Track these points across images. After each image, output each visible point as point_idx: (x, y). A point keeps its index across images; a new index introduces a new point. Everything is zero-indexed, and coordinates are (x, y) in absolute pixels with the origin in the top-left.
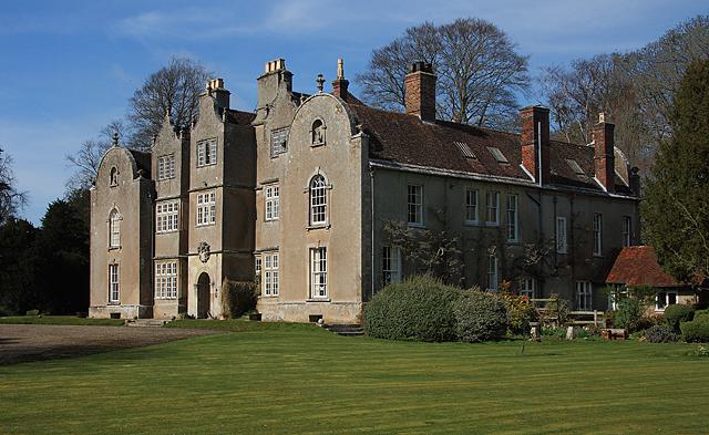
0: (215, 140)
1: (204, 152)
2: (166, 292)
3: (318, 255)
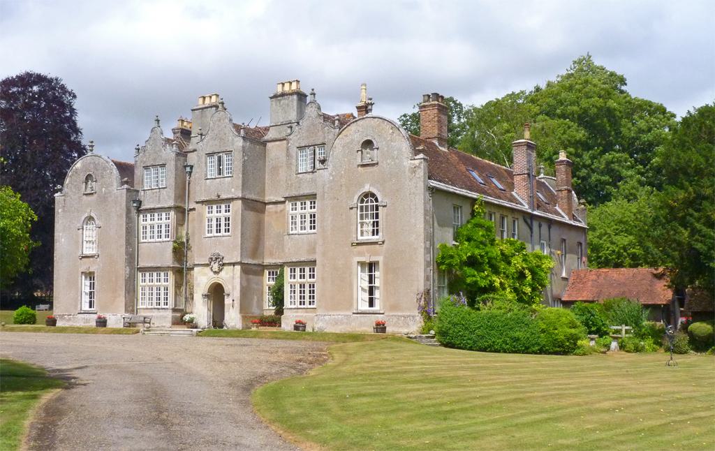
0: (229, 152)
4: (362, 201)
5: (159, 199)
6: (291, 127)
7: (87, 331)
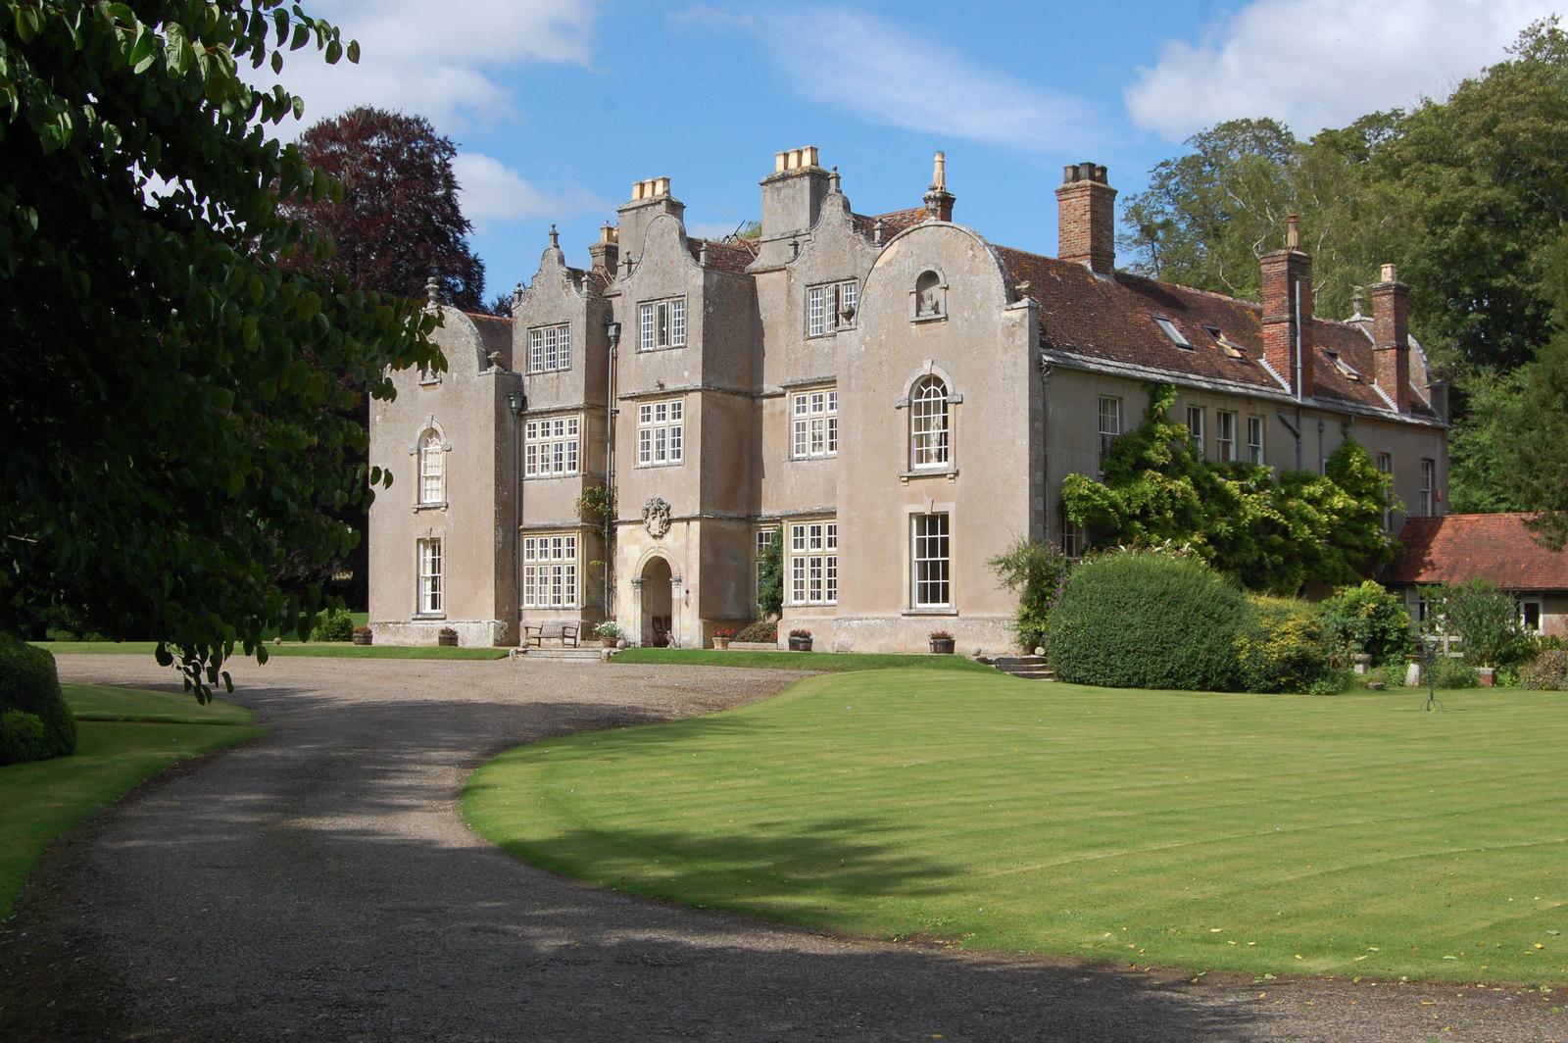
0: (679, 299)
1: (655, 322)
2: (550, 595)
3: (429, 552)
4: (920, 394)
5: (558, 393)
6: (796, 245)
7: (426, 654)
